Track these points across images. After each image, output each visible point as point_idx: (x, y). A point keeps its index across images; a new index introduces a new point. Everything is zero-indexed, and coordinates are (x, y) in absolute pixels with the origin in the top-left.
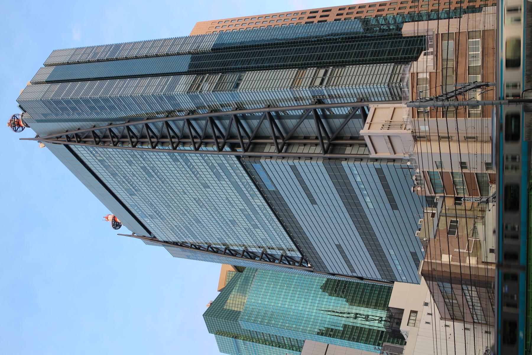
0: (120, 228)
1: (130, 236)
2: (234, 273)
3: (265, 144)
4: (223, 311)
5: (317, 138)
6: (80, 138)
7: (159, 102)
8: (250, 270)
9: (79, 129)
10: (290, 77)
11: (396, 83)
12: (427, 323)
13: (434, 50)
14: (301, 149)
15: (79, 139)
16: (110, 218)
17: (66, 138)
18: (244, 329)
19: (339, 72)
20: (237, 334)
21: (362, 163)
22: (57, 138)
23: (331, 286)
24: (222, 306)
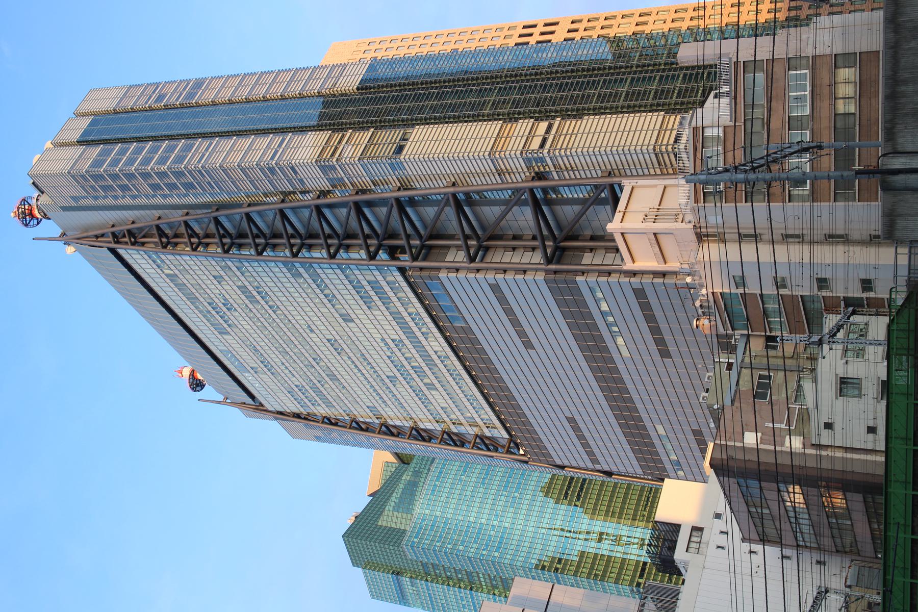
0: (202, 389)
1: (219, 402)
5: (534, 238)
6: (135, 238)
8: (422, 460)
12: (719, 547)
13: (731, 88)
14: (508, 257)
15: (133, 240)
16: (186, 372)
18: (411, 560)
22: (97, 237)
24: (375, 521)
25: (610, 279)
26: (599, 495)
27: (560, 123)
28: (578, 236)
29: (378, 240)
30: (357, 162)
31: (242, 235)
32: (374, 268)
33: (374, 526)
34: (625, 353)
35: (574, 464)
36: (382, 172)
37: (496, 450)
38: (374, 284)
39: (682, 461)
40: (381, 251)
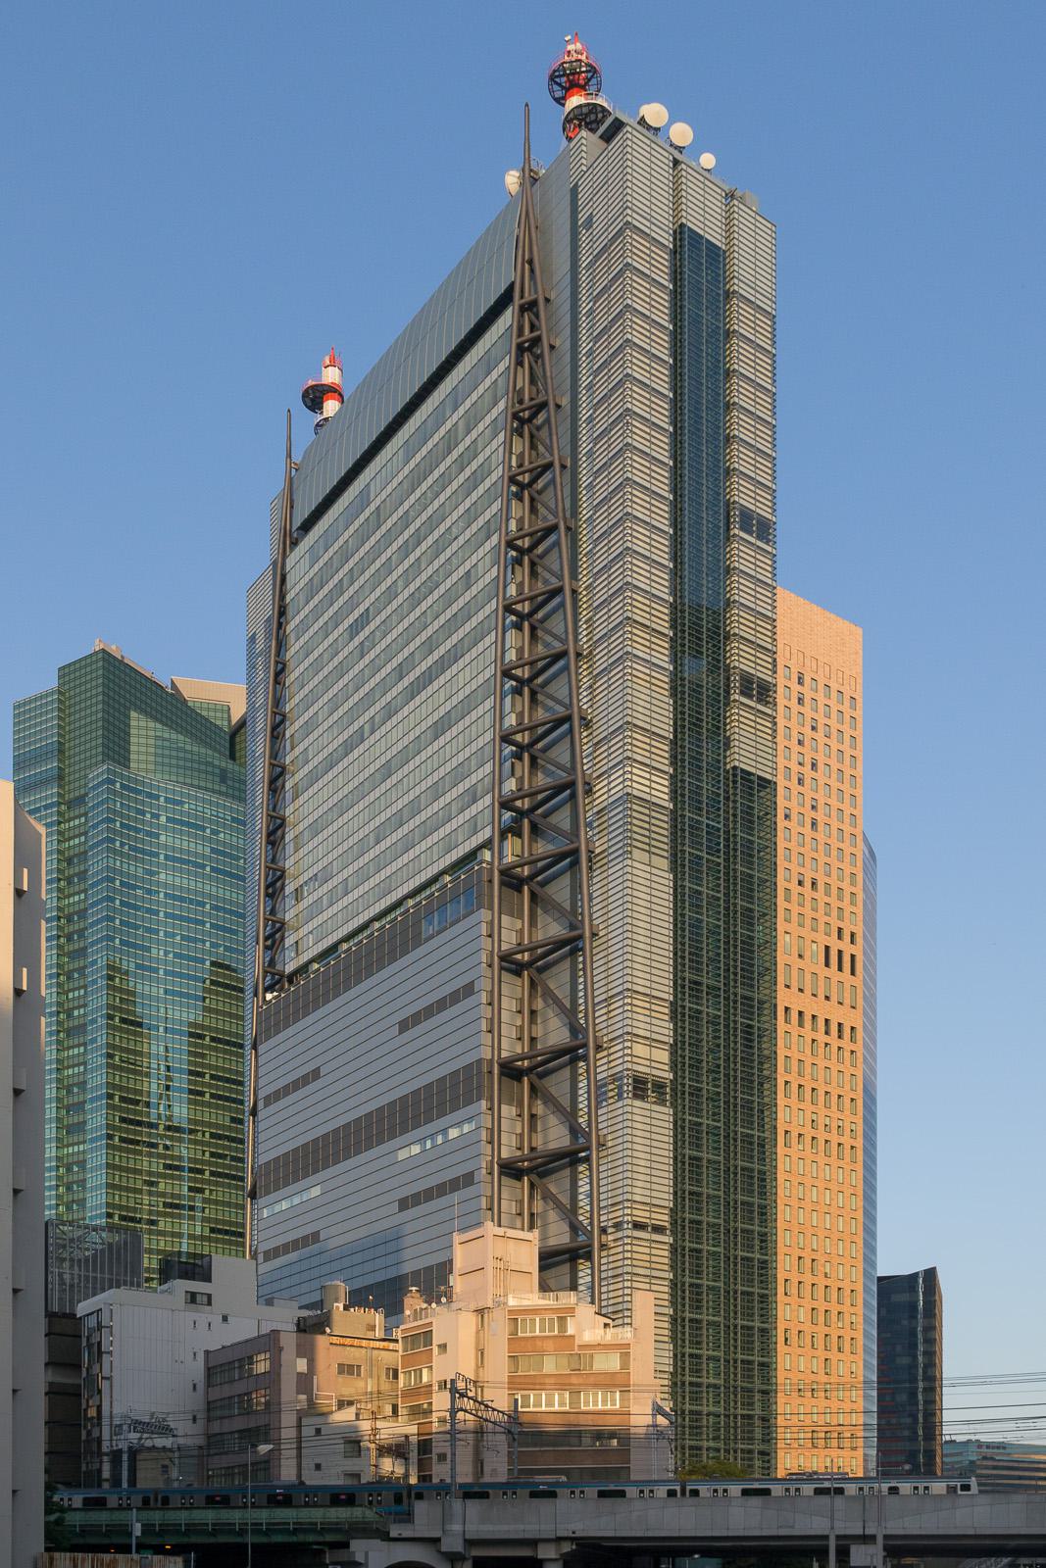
1: (289, 455)
2: (226, 723)
5: (532, 1149)
9: (552, 347)
10: (654, 722)
11: (631, 831)
14: (508, 1004)
18: (86, 776)
19: (662, 691)
20: (70, 757)
22: (531, 262)
24: (135, 705)
26: (224, 1013)
27: (666, 635)
30: (625, 615)
33: (128, 704)
37: (266, 948)
40: (514, 683)
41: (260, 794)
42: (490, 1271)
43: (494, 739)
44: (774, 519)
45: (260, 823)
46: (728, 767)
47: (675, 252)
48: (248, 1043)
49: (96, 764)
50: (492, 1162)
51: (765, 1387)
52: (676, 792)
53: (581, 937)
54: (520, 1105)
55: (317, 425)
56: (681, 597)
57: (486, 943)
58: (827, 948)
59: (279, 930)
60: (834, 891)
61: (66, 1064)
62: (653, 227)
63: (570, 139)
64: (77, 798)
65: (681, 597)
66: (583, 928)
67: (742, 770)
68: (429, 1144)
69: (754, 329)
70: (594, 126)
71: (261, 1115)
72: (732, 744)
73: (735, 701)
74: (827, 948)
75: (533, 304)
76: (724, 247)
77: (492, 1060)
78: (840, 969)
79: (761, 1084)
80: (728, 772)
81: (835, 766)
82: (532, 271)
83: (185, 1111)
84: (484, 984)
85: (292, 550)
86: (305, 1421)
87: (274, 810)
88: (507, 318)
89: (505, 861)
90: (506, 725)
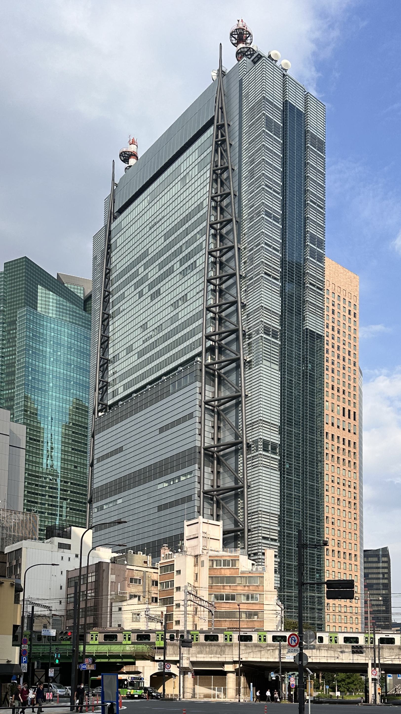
0: (122, 161)
1: (113, 180)
2: (82, 295)
3: (214, 386)
4: (34, 284)
5: (218, 487)
6: (221, 144)
7: (256, 210)
8: (88, 321)
9: (231, 145)
14: (209, 424)
16: (132, 148)
17: (222, 123)
18: (16, 312)
21: (198, 406)
22: (222, 108)
23: (80, 419)
25: (196, 483)
27: (277, 425)
28: (220, 465)
29: (218, 341)
31: (222, 238)
32: (204, 266)
33: (37, 282)
34: (160, 486)
35: (96, 442)
36: (255, 288)
38: (193, 266)
39: (102, 512)
41: (97, 327)
42: (201, 538)
43: (203, 337)
44: (324, 239)
45: (97, 339)
46: (304, 328)
47: (284, 111)
48: (90, 434)
49: (21, 307)
50: (200, 491)
51: (319, 607)
52: (282, 322)
53: (240, 396)
54: (213, 467)
55: (126, 169)
56: (285, 255)
57: (198, 396)
58: (344, 408)
59: (107, 363)
60: (347, 385)
61: (5, 388)
62: (274, 100)
63: (238, 60)
64: (11, 322)
65: (285, 255)
66: (242, 392)
67: (310, 330)
68: (172, 483)
69: (316, 163)
70: (249, 57)
71: (95, 466)
72: (306, 319)
73: (307, 287)
74: (344, 408)
75: (223, 125)
76: (304, 112)
77: (201, 446)
78: (349, 417)
79: (317, 463)
80: (304, 330)
81: (347, 333)
82: (222, 112)
83: (59, 464)
84: (197, 414)
85: (113, 221)
86: (113, 604)
87: (104, 333)
88: (211, 131)
89: (207, 362)
90: (208, 331)
